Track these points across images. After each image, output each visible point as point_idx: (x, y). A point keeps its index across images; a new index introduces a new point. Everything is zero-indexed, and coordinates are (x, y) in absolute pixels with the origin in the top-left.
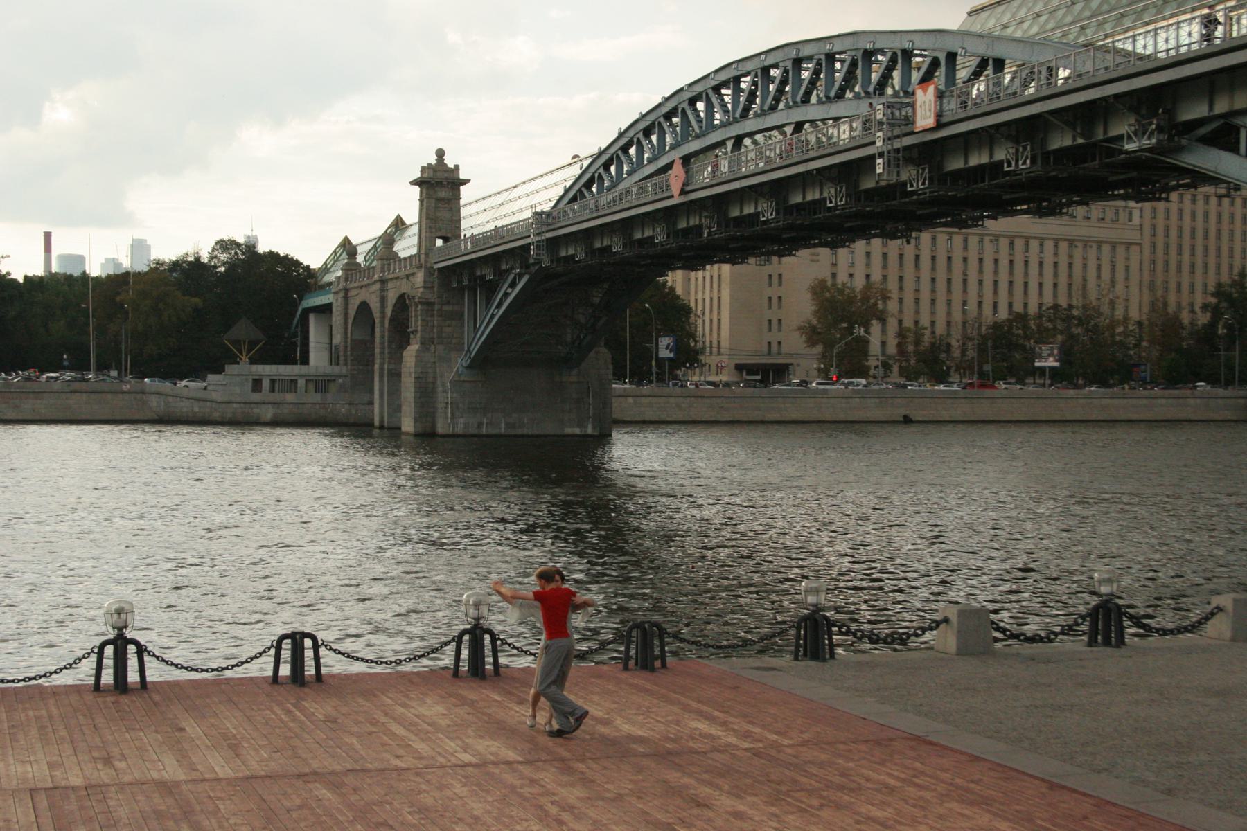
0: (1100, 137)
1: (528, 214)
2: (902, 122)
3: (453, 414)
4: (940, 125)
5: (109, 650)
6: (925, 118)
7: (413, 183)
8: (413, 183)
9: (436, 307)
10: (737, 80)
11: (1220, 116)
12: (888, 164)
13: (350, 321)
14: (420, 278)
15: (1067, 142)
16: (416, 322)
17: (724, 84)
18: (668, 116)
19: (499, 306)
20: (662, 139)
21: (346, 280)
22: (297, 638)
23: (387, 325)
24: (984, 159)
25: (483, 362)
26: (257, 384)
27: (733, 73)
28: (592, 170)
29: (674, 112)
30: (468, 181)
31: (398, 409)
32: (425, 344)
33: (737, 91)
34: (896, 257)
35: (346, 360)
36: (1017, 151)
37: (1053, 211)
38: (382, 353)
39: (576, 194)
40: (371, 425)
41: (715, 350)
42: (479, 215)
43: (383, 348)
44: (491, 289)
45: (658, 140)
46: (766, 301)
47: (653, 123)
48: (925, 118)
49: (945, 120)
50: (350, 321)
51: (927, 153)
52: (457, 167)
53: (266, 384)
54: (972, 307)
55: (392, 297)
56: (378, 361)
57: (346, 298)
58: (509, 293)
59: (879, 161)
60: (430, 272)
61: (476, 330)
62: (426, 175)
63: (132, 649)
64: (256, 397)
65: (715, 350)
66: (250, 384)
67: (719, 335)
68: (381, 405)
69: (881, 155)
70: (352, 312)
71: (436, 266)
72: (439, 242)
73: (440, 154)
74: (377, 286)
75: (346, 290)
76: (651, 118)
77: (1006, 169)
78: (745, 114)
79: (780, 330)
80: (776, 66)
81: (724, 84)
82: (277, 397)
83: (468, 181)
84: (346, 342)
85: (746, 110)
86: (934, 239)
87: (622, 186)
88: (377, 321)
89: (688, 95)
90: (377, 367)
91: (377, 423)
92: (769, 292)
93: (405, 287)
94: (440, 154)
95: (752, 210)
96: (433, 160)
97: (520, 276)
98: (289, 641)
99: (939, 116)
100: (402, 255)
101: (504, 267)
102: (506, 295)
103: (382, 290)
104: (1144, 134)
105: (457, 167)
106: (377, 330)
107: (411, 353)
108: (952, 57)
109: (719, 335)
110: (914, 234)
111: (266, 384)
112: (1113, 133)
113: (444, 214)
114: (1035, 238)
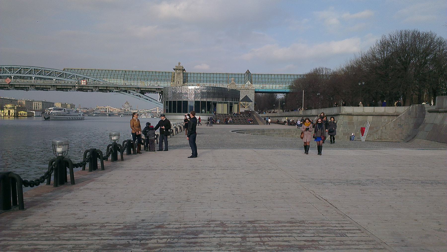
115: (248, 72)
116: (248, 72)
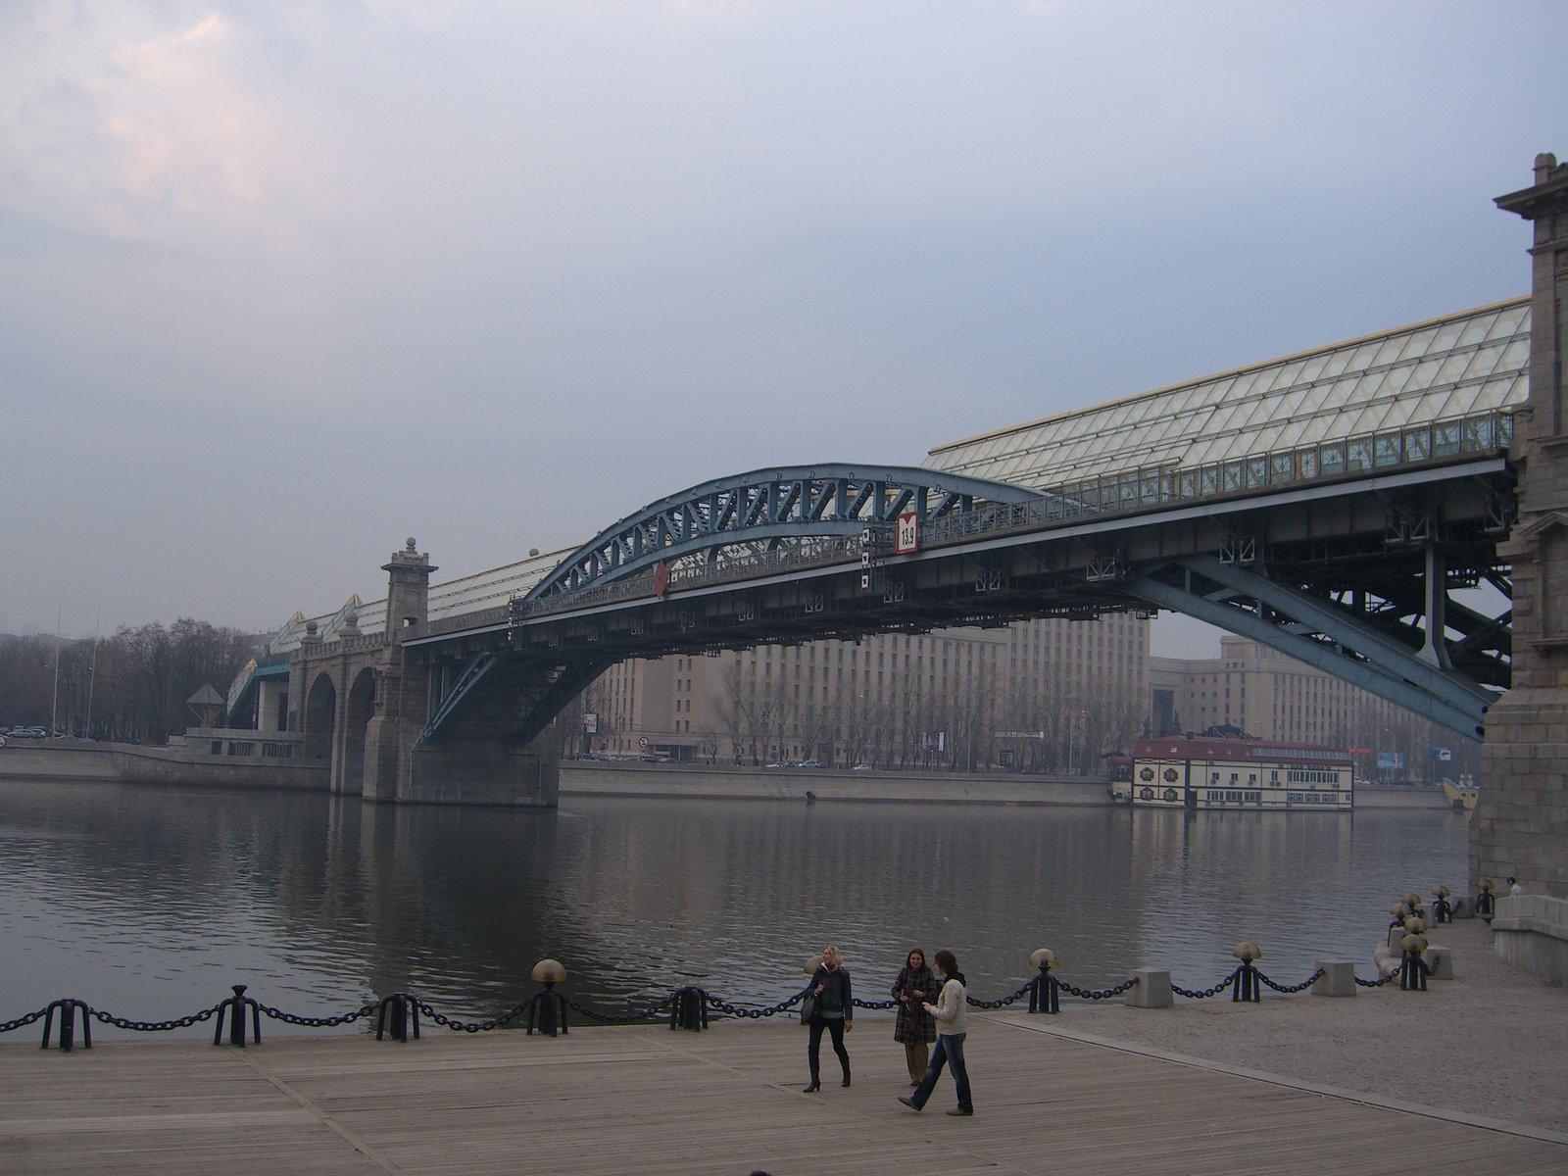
0: (1063, 568)
1: (504, 601)
2: (883, 544)
3: (413, 780)
4: (920, 550)
5: (229, 1009)
6: (906, 542)
7: (385, 568)
8: (385, 568)
9: (402, 682)
10: (715, 497)
11: (1168, 558)
12: (872, 582)
13: (308, 692)
14: (387, 654)
15: (1033, 571)
16: (382, 696)
17: (703, 499)
18: (645, 524)
19: (465, 684)
20: (638, 541)
21: (306, 652)
22: (67, 1007)
23: (347, 696)
24: (956, 580)
25: (441, 737)
26: (216, 747)
27: (713, 490)
28: (567, 566)
29: (654, 518)
30: (383, 568)
31: (360, 774)
32: (391, 714)
33: (715, 507)
34: (877, 655)
35: (302, 727)
36: (988, 575)
37: (995, 624)
38: (342, 721)
39: (549, 588)
40: (327, 790)
41: (627, 727)
42: (442, 604)
43: (342, 717)
44: (456, 669)
45: (635, 543)
46: (676, 684)
47: (631, 529)
48: (906, 542)
49: (924, 546)
50: (308, 692)
51: (905, 574)
52: (426, 556)
53: (225, 746)
54: (874, 695)
55: (355, 670)
56: (337, 729)
57: (304, 669)
58: (476, 674)
59: (866, 577)
60: (397, 649)
61: (439, 705)
62: (398, 561)
63: (249, 1008)
64: (215, 759)
65: (627, 727)
66: (210, 747)
67: (632, 712)
68: (339, 770)
69: (866, 571)
70: (311, 682)
71: (403, 645)
72: (406, 623)
73: (411, 544)
74: (340, 660)
75: (306, 662)
76: (630, 524)
77: (977, 590)
78: (722, 528)
79: (688, 710)
80: (755, 487)
81: (703, 499)
82: (236, 759)
83: (383, 568)
84: (303, 710)
85: (724, 523)
86: (920, 643)
87: (596, 584)
88: (338, 692)
89: (665, 507)
90: (336, 734)
91: (333, 786)
92: (679, 675)
93: (368, 662)
94: (411, 544)
95: (729, 611)
96: (404, 547)
97: (488, 658)
98: (60, 1007)
99: (919, 542)
100: (365, 632)
101: (472, 649)
102: (473, 674)
103: (345, 664)
104: (1104, 567)
105: (426, 556)
106: (338, 700)
107: (376, 723)
108: (923, 491)
109: (632, 712)
110: (864, 637)
111: (225, 746)
112: (1073, 565)
113: (412, 599)
114: (989, 643)
115: (1535, 169)
116: (1535, 169)
